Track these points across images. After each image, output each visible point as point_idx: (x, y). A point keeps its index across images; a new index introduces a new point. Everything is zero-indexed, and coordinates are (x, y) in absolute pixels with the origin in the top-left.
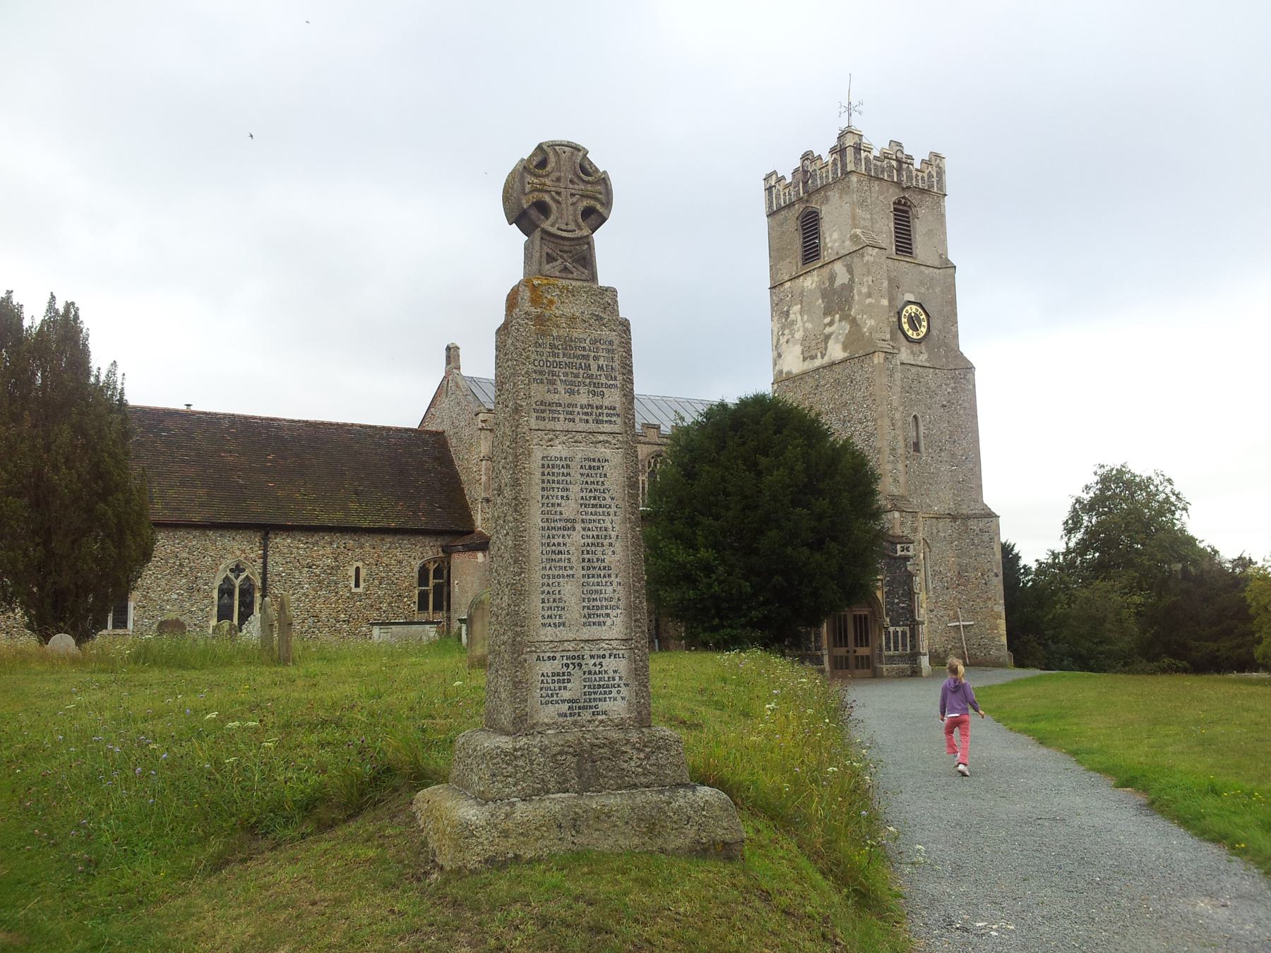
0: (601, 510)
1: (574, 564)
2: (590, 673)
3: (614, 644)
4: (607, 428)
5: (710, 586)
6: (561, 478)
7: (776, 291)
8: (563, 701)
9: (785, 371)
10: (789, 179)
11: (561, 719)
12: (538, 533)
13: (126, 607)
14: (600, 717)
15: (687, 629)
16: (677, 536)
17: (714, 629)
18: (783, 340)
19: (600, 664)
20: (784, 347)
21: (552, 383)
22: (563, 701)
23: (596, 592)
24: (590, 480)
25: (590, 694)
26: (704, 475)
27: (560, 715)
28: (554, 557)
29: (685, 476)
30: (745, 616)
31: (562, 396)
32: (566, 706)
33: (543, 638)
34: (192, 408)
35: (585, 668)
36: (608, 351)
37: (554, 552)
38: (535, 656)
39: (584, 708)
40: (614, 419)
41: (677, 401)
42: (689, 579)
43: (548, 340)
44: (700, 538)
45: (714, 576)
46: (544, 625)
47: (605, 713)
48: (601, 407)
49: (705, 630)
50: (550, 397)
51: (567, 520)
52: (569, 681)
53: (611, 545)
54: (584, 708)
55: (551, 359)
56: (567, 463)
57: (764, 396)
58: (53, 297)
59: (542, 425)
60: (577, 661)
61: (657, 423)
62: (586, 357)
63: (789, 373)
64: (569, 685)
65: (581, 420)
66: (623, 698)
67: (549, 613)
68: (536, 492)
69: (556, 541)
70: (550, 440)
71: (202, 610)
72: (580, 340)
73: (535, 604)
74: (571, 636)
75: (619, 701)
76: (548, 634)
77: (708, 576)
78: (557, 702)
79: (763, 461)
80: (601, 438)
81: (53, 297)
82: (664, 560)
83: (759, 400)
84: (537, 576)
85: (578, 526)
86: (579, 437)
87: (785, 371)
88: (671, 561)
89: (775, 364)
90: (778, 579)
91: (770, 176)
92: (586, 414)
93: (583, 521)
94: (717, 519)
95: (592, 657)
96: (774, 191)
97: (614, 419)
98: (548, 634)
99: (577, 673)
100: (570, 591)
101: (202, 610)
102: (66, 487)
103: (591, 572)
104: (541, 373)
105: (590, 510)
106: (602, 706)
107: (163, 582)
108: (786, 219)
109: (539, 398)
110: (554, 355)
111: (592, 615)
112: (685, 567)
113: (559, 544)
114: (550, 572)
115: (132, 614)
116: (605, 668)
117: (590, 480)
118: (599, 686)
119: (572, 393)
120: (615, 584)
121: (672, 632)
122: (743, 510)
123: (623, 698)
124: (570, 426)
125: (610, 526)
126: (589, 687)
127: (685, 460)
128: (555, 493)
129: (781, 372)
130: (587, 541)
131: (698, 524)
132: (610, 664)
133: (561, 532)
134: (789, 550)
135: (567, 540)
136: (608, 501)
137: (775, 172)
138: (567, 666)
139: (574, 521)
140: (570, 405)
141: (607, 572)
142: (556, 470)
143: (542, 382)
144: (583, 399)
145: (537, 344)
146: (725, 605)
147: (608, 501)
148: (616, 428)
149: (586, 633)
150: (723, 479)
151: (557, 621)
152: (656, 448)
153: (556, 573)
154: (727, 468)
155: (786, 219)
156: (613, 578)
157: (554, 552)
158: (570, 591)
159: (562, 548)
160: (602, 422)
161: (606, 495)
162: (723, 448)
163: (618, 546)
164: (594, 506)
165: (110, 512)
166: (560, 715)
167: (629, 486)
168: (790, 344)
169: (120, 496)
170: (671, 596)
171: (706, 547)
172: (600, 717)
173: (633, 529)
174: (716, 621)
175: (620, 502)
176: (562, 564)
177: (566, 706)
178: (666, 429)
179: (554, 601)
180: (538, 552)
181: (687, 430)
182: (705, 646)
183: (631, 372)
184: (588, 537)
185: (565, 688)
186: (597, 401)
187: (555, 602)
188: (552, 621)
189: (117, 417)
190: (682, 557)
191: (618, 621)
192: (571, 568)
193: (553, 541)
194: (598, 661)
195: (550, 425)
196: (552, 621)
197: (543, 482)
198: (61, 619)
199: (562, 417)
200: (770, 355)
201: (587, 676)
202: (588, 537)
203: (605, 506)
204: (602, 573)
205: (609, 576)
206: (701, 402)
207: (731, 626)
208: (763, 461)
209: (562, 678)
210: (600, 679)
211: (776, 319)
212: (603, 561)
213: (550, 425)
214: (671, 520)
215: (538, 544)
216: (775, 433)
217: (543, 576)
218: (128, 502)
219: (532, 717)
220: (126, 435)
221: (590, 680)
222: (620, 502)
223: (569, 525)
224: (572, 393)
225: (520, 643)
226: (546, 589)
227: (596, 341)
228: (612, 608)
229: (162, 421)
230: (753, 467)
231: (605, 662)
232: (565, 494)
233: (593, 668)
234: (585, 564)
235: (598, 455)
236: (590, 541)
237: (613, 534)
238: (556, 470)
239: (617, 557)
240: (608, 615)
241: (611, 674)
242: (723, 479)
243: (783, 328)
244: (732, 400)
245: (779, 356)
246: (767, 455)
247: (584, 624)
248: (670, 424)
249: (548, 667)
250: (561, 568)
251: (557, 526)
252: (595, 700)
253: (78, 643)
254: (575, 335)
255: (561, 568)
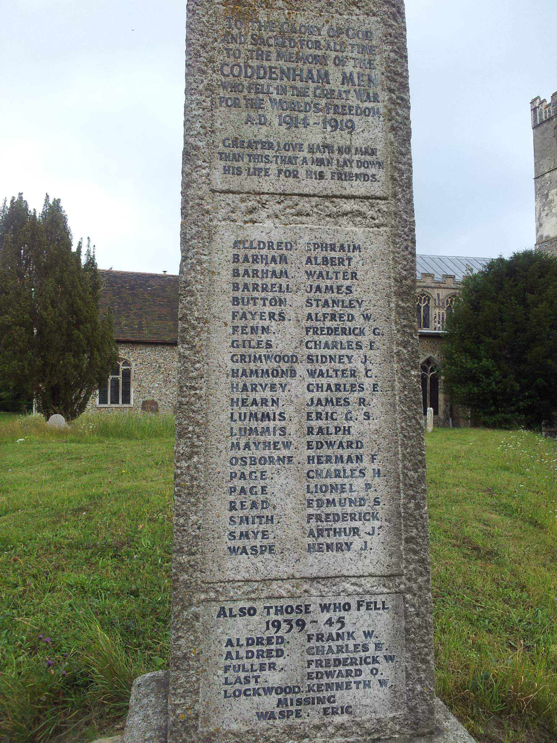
0: (344, 339)
1: (293, 438)
2: (320, 637)
3: (367, 583)
4: (359, 188)
5: (489, 384)
6: (269, 281)
7: (539, 180)
8: (268, 691)
9: (545, 235)
10: (549, 101)
11: (263, 724)
12: (224, 382)
13: (129, 392)
14: (338, 719)
15: (472, 412)
16: (466, 350)
17: (492, 414)
18: (543, 214)
19: (341, 621)
20: (545, 219)
21: (255, 105)
22: (268, 691)
23: (334, 488)
24: (323, 283)
25: (319, 676)
26: (486, 308)
27: (261, 716)
28: (254, 424)
29: (472, 309)
30: (514, 405)
31: (274, 129)
32: (273, 699)
33: (231, 575)
34: (167, 273)
35: (310, 629)
36: (363, 49)
37: (253, 416)
38: (215, 608)
39: (308, 702)
40: (372, 171)
41: (466, 259)
42: (474, 379)
43: (251, 28)
44: (482, 352)
45: (492, 378)
46: (233, 550)
47: (347, 710)
48: (348, 150)
49: (485, 414)
50: (250, 132)
51: (281, 358)
52: (280, 653)
53: (362, 401)
54: (308, 702)
55: (254, 63)
56: (280, 253)
57: (531, 252)
58: (48, 196)
59: (235, 182)
60: (296, 616)
61: (452, 274)
62: (321, 60)
63: (547, 237)
64: (280, 662)
65: (309, 173)
66: (382, 683)
67: (244, 528)
68: (222, 307)
69: (258, 396)
70: (252, 211)
71: (172, 393)
72: (310, 30)
73: (217, 512)
74: (284, 570)
75: (376, 690)
76: (241, 567)
77: (487, 378)
78: (256, 692)
79: (530, 297)
80: (348, 206)
81: (48, 196)
82: (457, 366)
83: (527, 255)
84: (221, 462)
85: (301, 369)
86: (305, 205)
87: (545, 235)
88: (462, 367)
89: (537, 231)
90: (540, 381)
91: (535, 100)
92: (320, 162)
93: (310, 359)
94: (495, 338)
95: (325, 608)
96: (538, 110)
97: (372, 171)
98: (241, 567)
99: (296, 638)
100: (284, 487)
101: (172, 393)
102: (52, 319)
103: (326, 451)
104: (235, 87)
105: (323, 339)
106: (343, 697)
107: (150, 377)
108: (547, 129)
109: (231, 132)
110: (260, 57)
111: (325, 532)
112: (471, 372)
113: (264, 402)
114: (247, 453)
115: (132, 395)
116: (349, 628)
117: (323, 283)
118: (338, 662)
119: (292, 123)
120: (369, 473)
121: (461, 414)
122: (516, 332)
123: (382, 683)
124: (290, 185)
125: (361, 368)
126: (319, 663)
127: (473, 298)
128: (259, 308)
129: (542, 237)
130: (316, 395)
131: (481, 342)
132: (358, 621)
133: (268, 380)
134: (549, 361)
135: (279, 394)
136: (359, 322)
137: (538, 97)
138: (277, 625)
139: (293, 359)
140: (287, 146)
141: (354, 452)
142: (260, 267)
143: (236, 104)
144: (314, 135)
145: (229, 37)
146: (499, 398)
147: (359, 322)
148: (376, 189)
149: (315, 564)
150: (500, 311)
151: (258, 542)
152: (452, 291)
153: (258, 454)
154: (503, 303)
155: (547, 129)
156: (366, 463)
157: (253, 416)
158: (284, 487)
159: (270, 409)
160: (349, 177)
161: (356, 312)
162: (501, 289)
163: (377, 405)
164: (332, 331)
165: (81, 336)
166: (261, 716)
167: (398, 294)
168: (549, 216)
169: (88, 325)
170: (461, 391)
171: (487, 358)
172: (338, 719)
173: (405, 373)
174: (493, 408)
175: (381, 324)
176: (270, 438)
177: (273, 699)
178: (459, 278)
179: (254, 505)
180: (225, 417)
181: (475, 277)
182: (486, 425)
183: (404, 87)
184: (319, 387)
185: (272, 666)
186: (340, 138)
187: (255, 509)
188: (248, 543)
189: (88, 275)
190: (469, 364)
191: (375, 541)
192: (287, 445)
193: (252, 396)
194: (335, 616)
195: (251, 183)
196: (248, 543)
197: (236, 287)
198: (57, 405)
199: (273, 168)
200: (533, 226)
201: (314, 643)
202: (319, 387)
203: (352, 331)
204: (345, 453)
205: (359, 458)
206: (484, 259)
207: (503, 412)
208: (530, 297)
209: (266, 648)
210: (340, 649)
211: (538, 200)
212: (347, 431)
213: (251, 183)
214: (462, 339)
215: (225, 401)
216: (540, 277)
217: (233, 461)
218: (94, 329)
219: (206, 720)
220: (96, 287)
221: (320, 651)
222: (381, 324)
223: (284, 366)
224: (292, 123)
225: (187, 585)
226: (238, 483)
227: (340, 31)
228: (363, 517)
229: (147, 281)
230: (523, 301)
231: (348, 617)
232: (276, 310)
233: (326, 630)
234: (314, 438)
235: (340, 238)
236: (323, 395)
237: (368, 382)
238: (260, 267)
239: (374, 424)
240: (355, 531)
241: (360, 639)
242: (500, 311)
243: (544, 206)
244: (507, 256)
245: (541, 225)
246: (533, 293)
247: (310, 548)
248: (461, 275)
249: (240, 628)
250: (267, 445)
251: (259, 367)
252: (329, 686)
253: (67, 419)
254: (301, 20)
255: (267, 445)
